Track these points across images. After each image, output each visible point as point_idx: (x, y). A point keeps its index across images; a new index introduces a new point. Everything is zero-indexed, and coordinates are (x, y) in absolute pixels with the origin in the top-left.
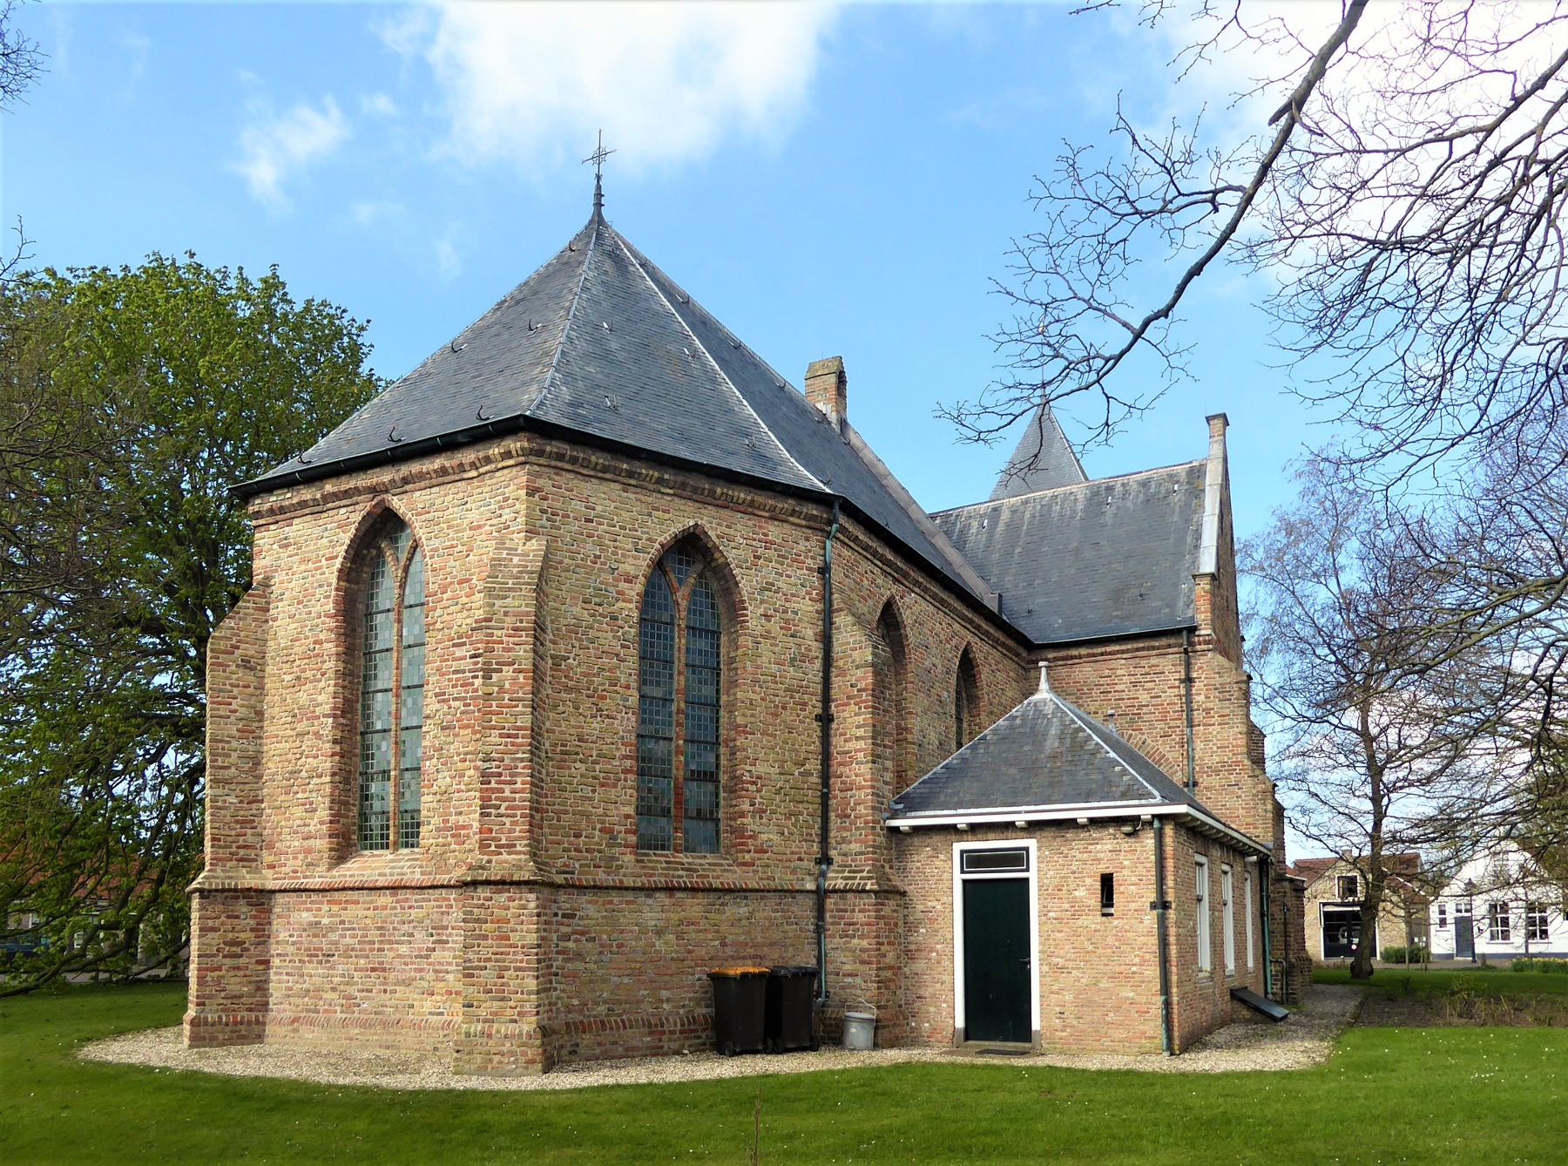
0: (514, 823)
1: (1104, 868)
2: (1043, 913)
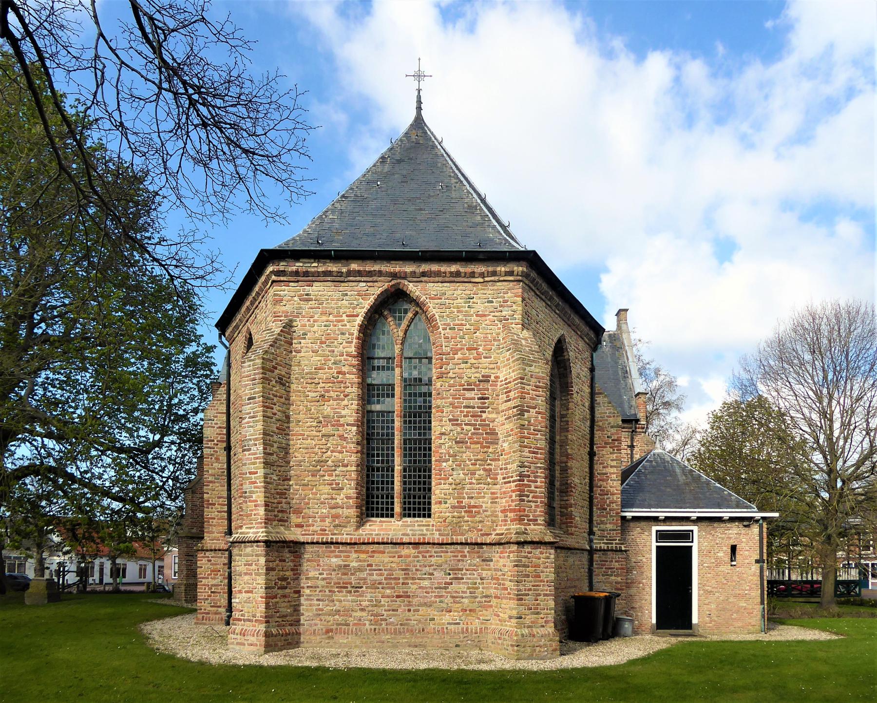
0: (537, 506)
1: (732, 542)
2: (700, 564)
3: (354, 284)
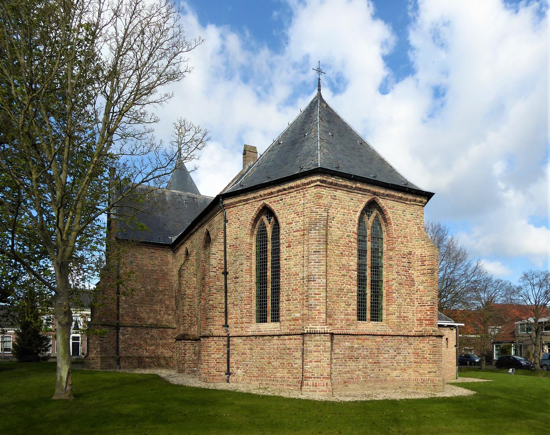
3: (356, 194)
